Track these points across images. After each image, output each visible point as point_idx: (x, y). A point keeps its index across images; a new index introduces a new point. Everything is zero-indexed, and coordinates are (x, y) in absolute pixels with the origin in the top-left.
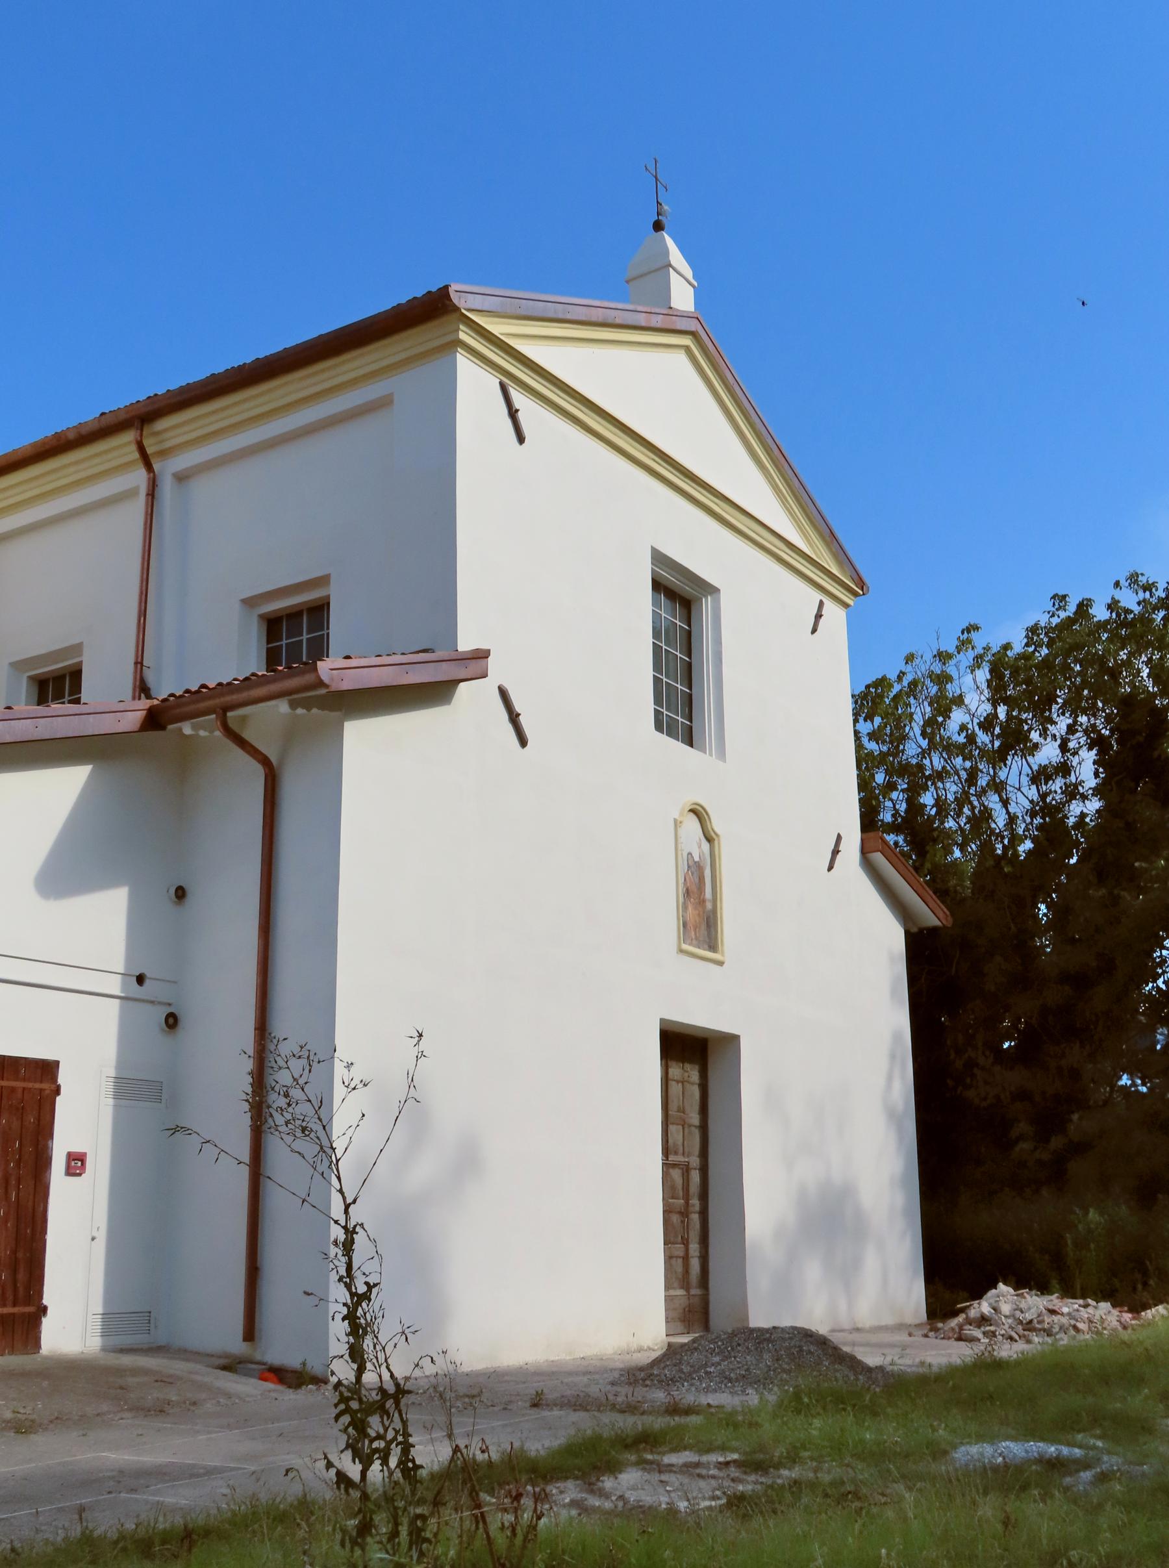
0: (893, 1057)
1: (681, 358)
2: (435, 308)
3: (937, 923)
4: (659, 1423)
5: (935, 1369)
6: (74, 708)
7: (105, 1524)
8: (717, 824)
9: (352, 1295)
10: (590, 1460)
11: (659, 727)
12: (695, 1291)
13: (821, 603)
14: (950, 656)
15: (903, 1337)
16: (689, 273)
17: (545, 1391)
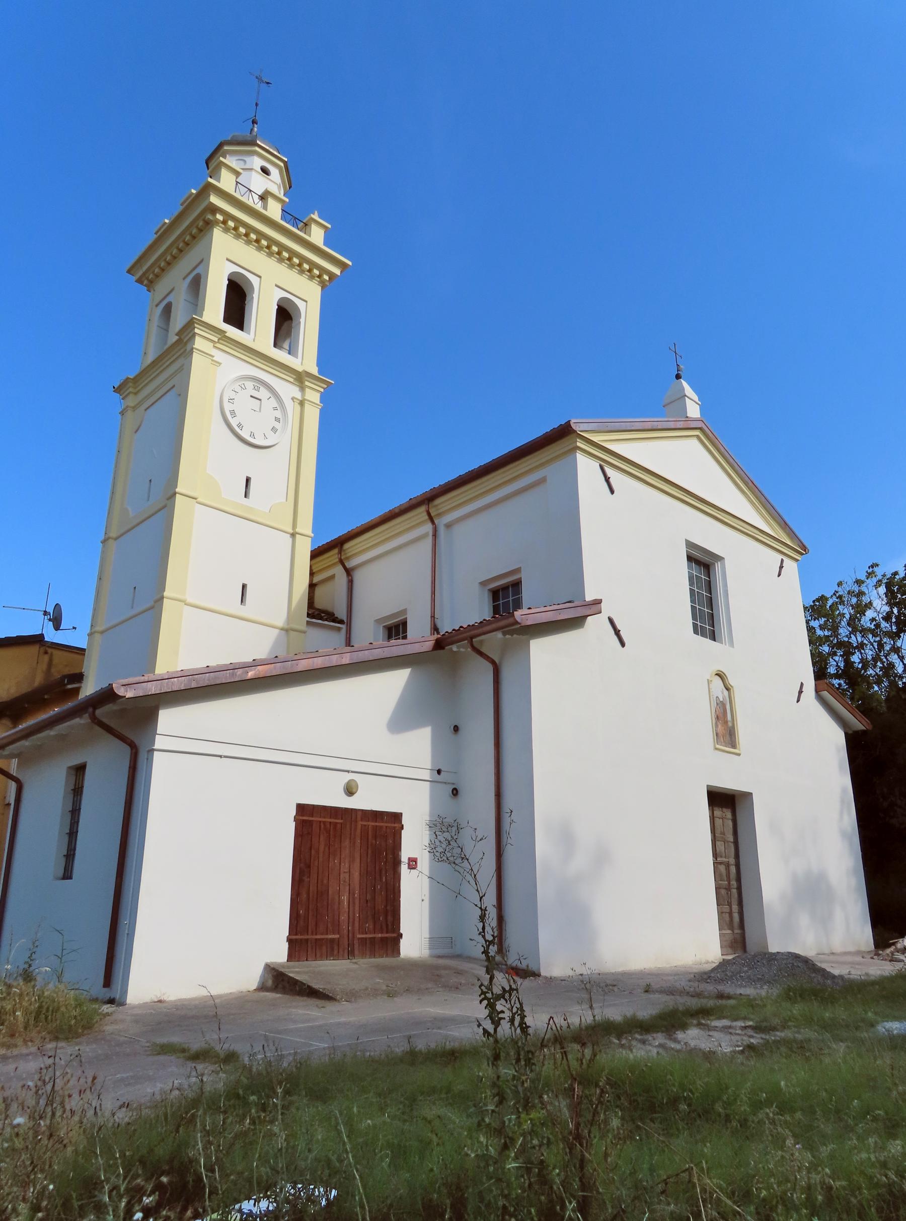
0: (842, 801)
1: (695, 441)
2: (564, 432)
3: (861, 727)
4: (711, 1003)
5: (872, 978)
6: (401, 641)
7: (421, 1045)
8: (731, 681)
9: (486, 941)
10: (670, 1022)
11: (696, 632)
12: (737, 931)
13: (782, 560)
14: (863, 582)
15: (859, 959)
16: (696, 398)
17: (652, 984)
